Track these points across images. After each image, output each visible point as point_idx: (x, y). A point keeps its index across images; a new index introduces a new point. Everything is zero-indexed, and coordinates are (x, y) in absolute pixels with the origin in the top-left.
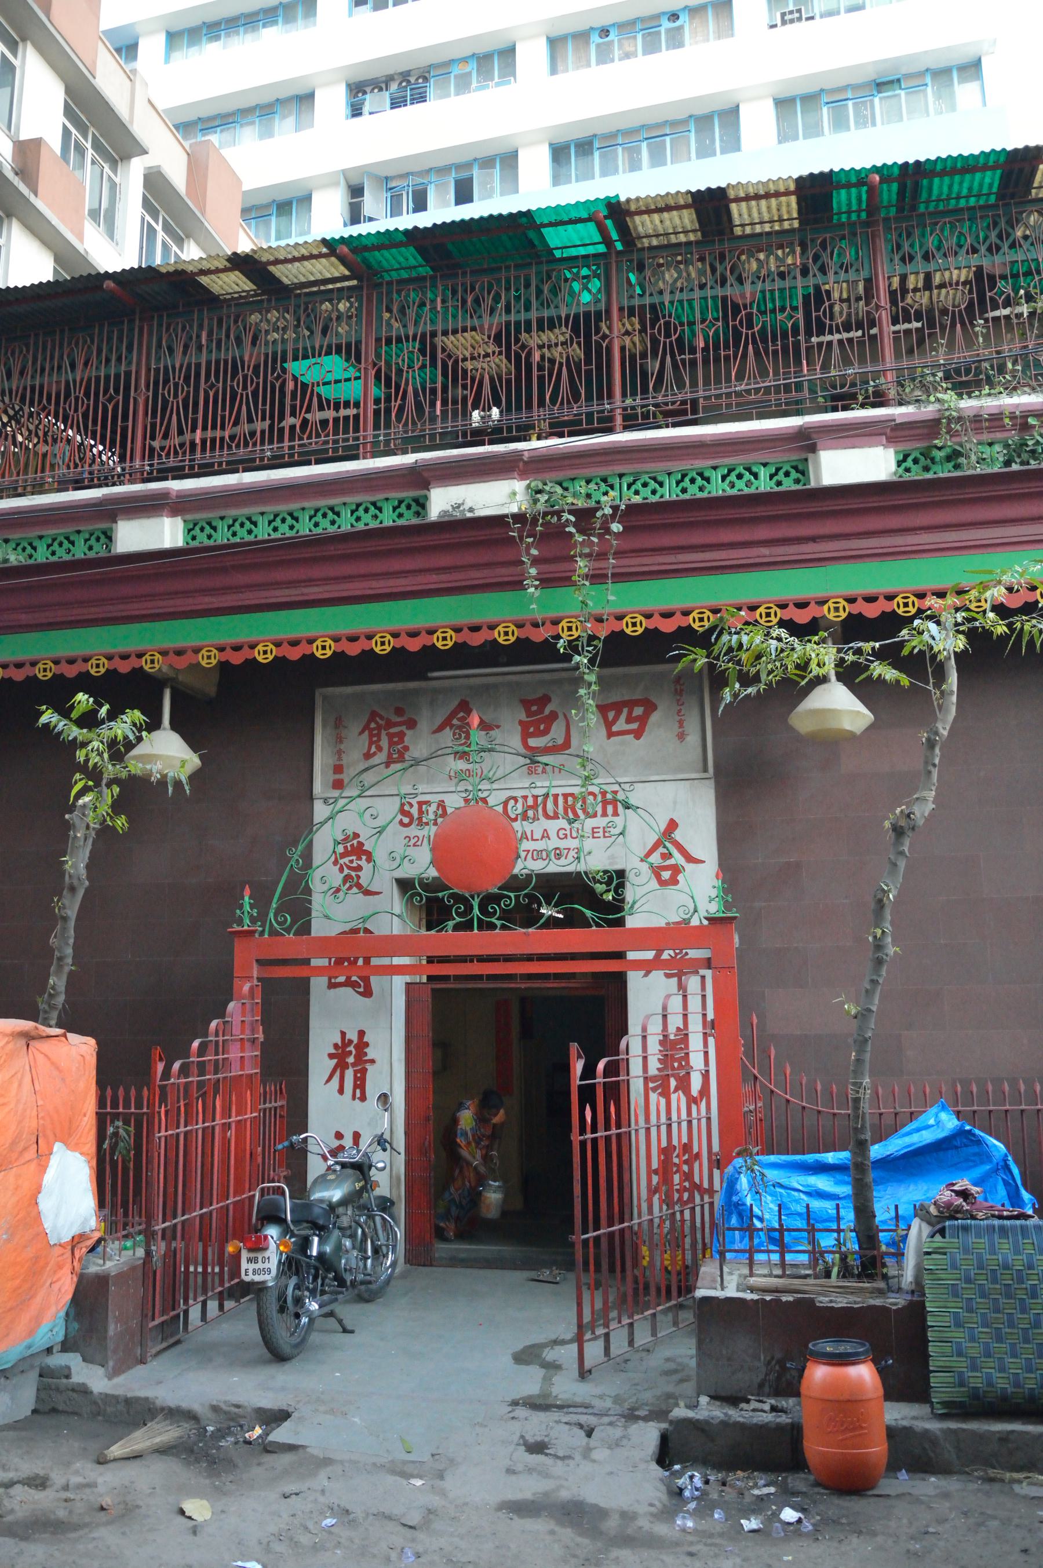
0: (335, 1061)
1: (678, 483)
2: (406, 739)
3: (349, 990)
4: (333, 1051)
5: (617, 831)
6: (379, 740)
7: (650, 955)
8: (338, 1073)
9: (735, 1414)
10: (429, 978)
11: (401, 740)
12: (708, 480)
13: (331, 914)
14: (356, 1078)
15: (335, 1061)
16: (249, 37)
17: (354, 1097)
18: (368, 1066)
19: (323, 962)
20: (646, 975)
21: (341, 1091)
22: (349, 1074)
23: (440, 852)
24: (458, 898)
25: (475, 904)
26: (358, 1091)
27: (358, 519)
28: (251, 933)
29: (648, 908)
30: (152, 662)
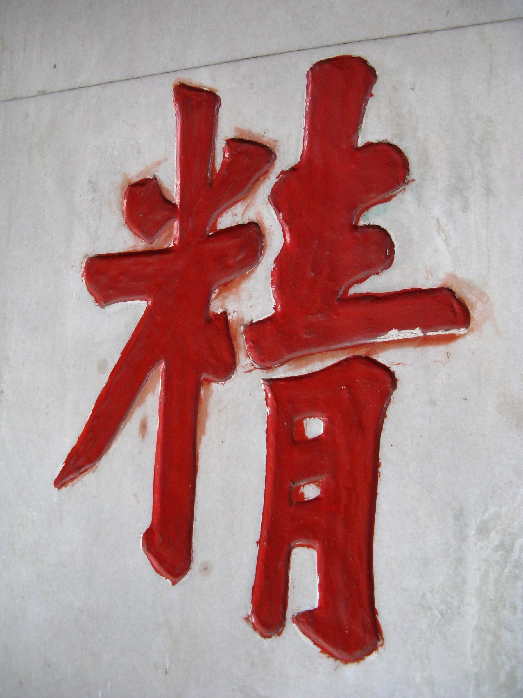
0: (130, 313)
4: (121, 239)
8: (149, 407)
9: (311, 544)
15: (130, 313)
16: (268, 238)
17: (268, 608)
18: (402, 355)
21: (170, 542)
22: (237, 415)
26: (304, 566)
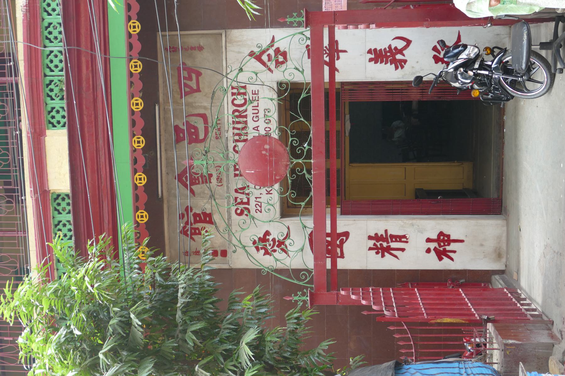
0: (386, 254)
1: (51, 42)
2: (198, 212)
3: (345, 245)
5: (254, 77)
6: (198, 229)
7: (326, 69)
8: (392, 252)
10: (338, 158)
11: (199, 215)
12: (50, 24)
13: (299, 256)
14: (396, 241)
15: (386, 254)
17: (407, 242)
18: (389, 233)
19: (329, 262)
20: (338, 71)
21: (403, 250)
22: (394, 245)
23: (264, 181)
24: (293, 171)
25: (295, 161)
26: (403, 240)
27: (56, 38)
28: (312, 295)
29: (299, 69)
30: (137, 104)
